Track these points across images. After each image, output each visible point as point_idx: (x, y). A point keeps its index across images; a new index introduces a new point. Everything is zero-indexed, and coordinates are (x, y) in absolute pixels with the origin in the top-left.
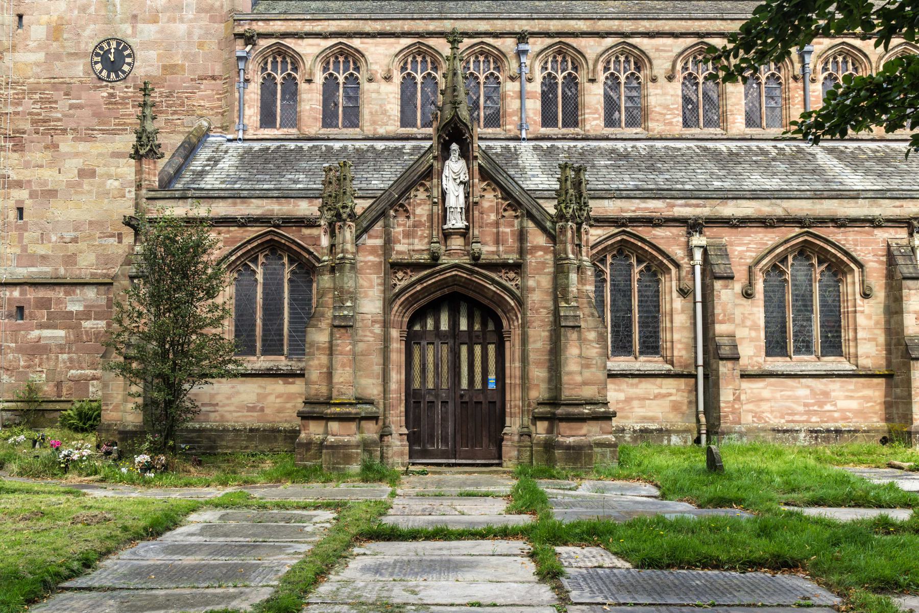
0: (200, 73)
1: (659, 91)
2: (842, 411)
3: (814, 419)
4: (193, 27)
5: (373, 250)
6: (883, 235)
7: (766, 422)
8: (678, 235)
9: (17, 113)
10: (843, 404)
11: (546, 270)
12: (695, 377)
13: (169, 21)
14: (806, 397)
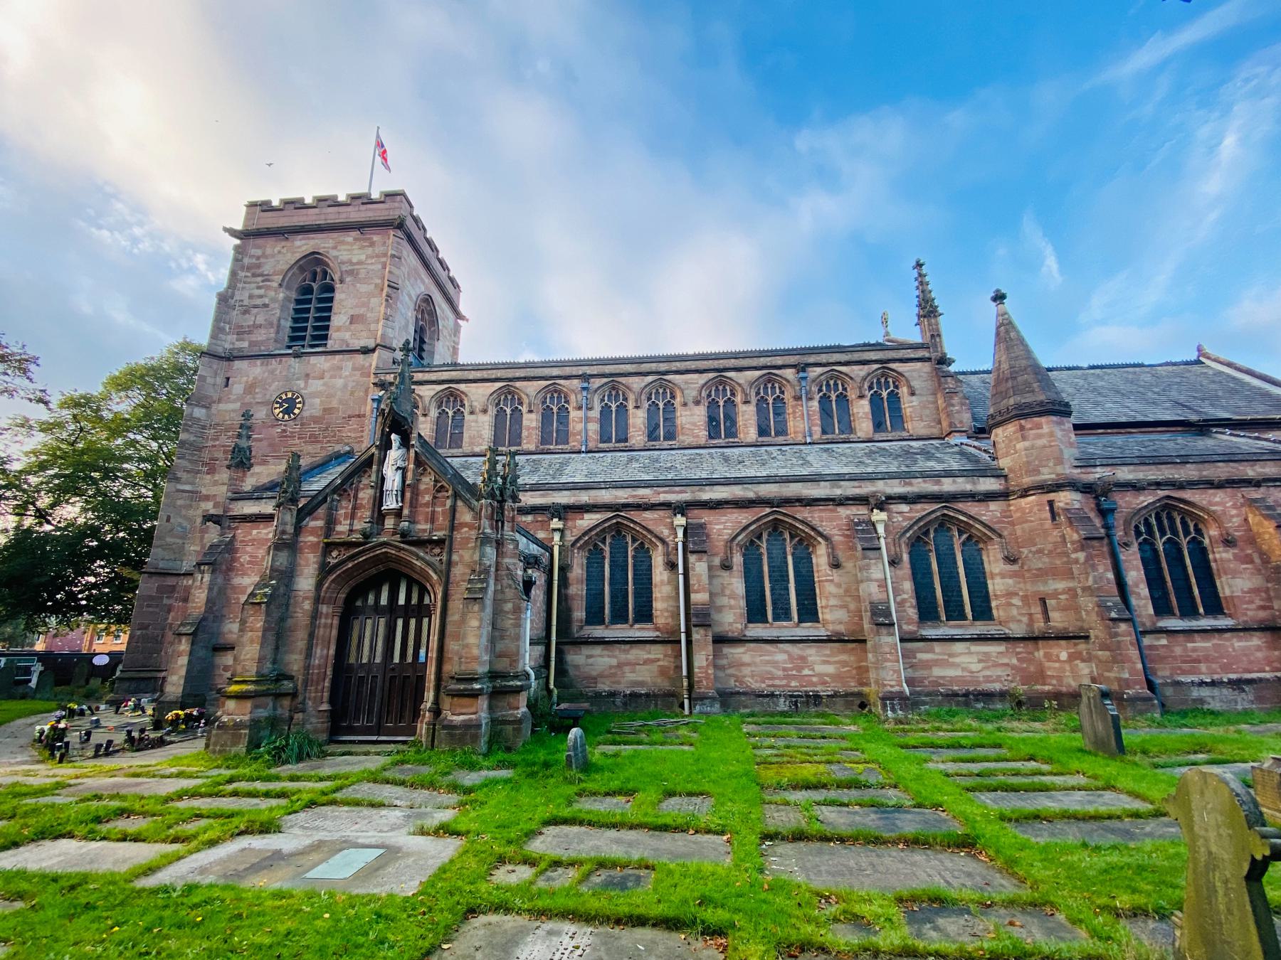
0: (350, 413)
1: (688, 413)
2: (820, 675)
3: (793, 684)
5: (313, 532)
6: (843, 512)
7: (748, 686)
9: (215, 446)
10: (820, 668)
12: (679, 642)
13: (331, 377)
14: (785, 662)
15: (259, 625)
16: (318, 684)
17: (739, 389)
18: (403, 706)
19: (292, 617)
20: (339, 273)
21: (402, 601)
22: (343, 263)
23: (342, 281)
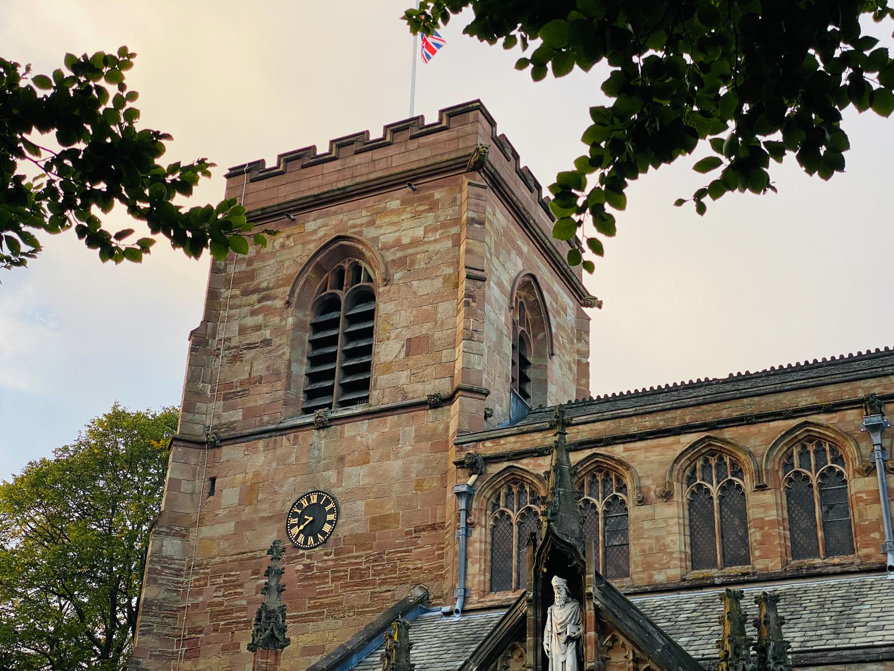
0: (417, 522)
4: (412, 463)
9: (195, 606)
13: (381, 459)
20: (383, 270)
22: (386, 248)
23: (387, 281)
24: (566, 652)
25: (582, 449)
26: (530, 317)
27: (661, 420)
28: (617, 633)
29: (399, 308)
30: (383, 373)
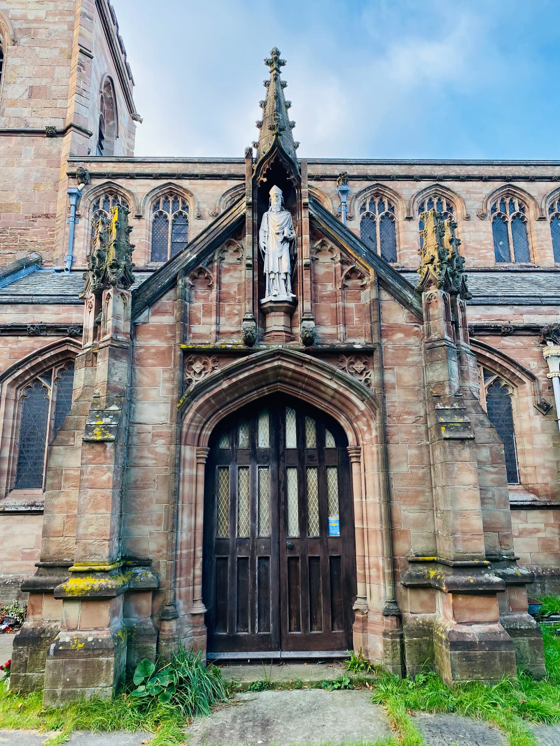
1: (472, 228)
4: (30, 171)
5: (158, 332)
8: (530, 346)
11: (410, 360)
15: (105, 478)
16: (188, 573)
17: (531, 203)
18: (314, 606)
19: (136, 466)
20: (12, 33)
21: (291, 442)
23: (14, 42)
24: (282, 249)
25: (161, 179)
26: (106, 109)
27: (215, 169)
28: (326, 239)
29: (24, 63)
30: (10, 106)
